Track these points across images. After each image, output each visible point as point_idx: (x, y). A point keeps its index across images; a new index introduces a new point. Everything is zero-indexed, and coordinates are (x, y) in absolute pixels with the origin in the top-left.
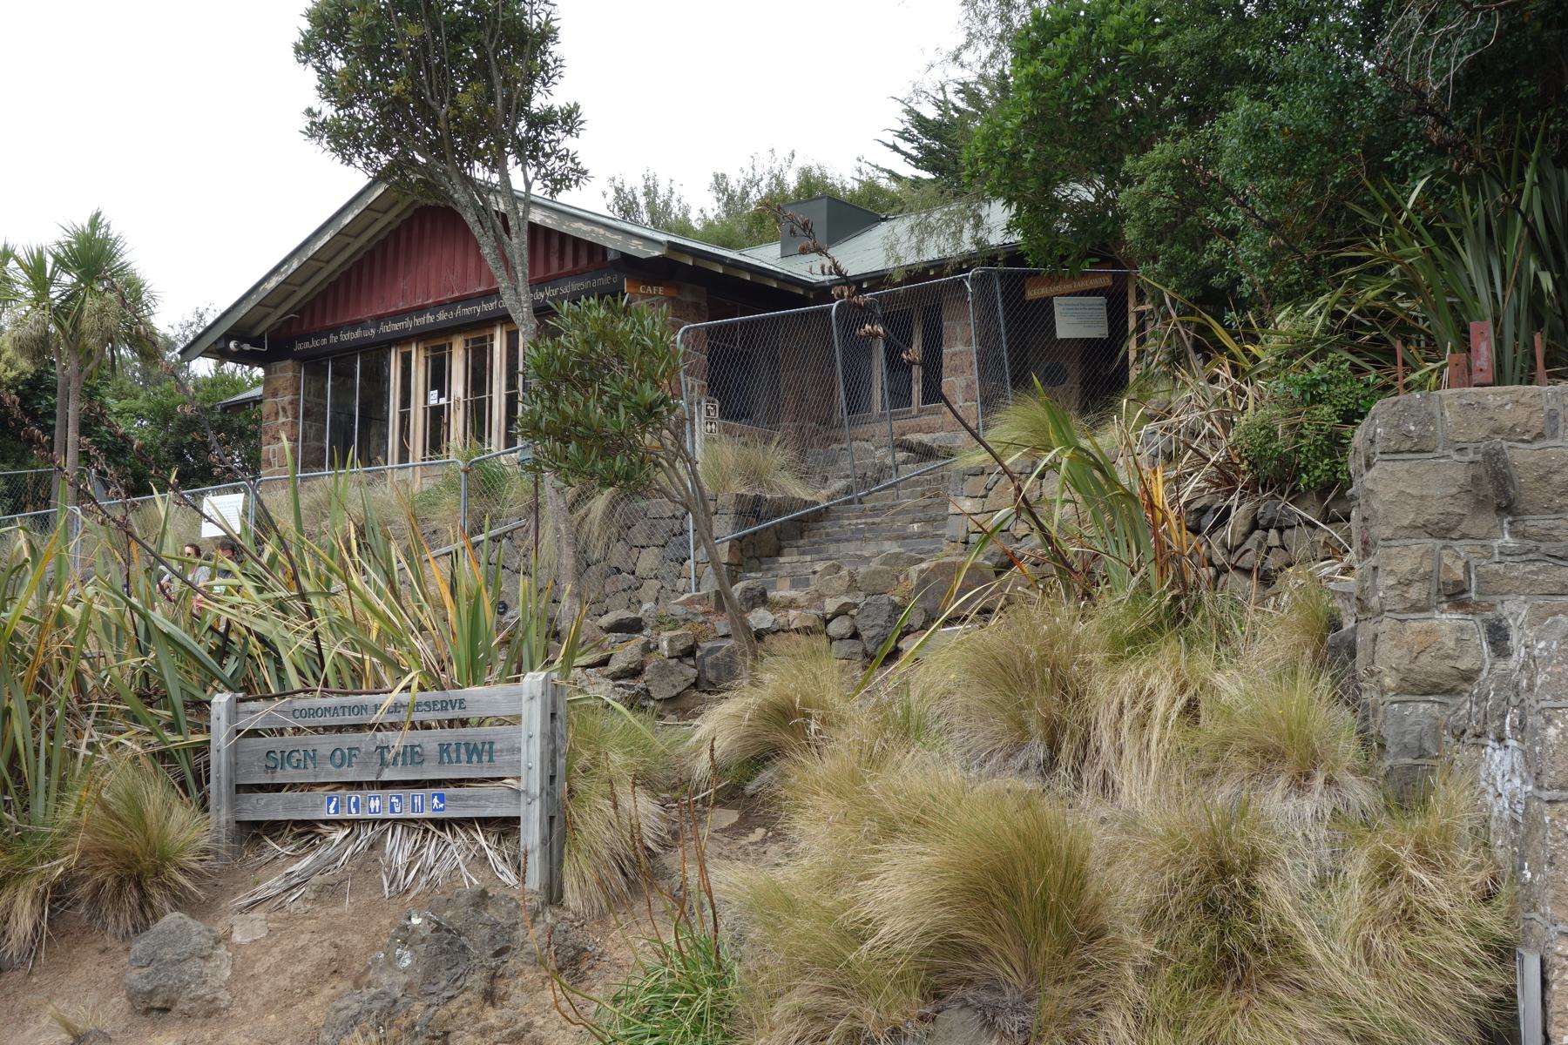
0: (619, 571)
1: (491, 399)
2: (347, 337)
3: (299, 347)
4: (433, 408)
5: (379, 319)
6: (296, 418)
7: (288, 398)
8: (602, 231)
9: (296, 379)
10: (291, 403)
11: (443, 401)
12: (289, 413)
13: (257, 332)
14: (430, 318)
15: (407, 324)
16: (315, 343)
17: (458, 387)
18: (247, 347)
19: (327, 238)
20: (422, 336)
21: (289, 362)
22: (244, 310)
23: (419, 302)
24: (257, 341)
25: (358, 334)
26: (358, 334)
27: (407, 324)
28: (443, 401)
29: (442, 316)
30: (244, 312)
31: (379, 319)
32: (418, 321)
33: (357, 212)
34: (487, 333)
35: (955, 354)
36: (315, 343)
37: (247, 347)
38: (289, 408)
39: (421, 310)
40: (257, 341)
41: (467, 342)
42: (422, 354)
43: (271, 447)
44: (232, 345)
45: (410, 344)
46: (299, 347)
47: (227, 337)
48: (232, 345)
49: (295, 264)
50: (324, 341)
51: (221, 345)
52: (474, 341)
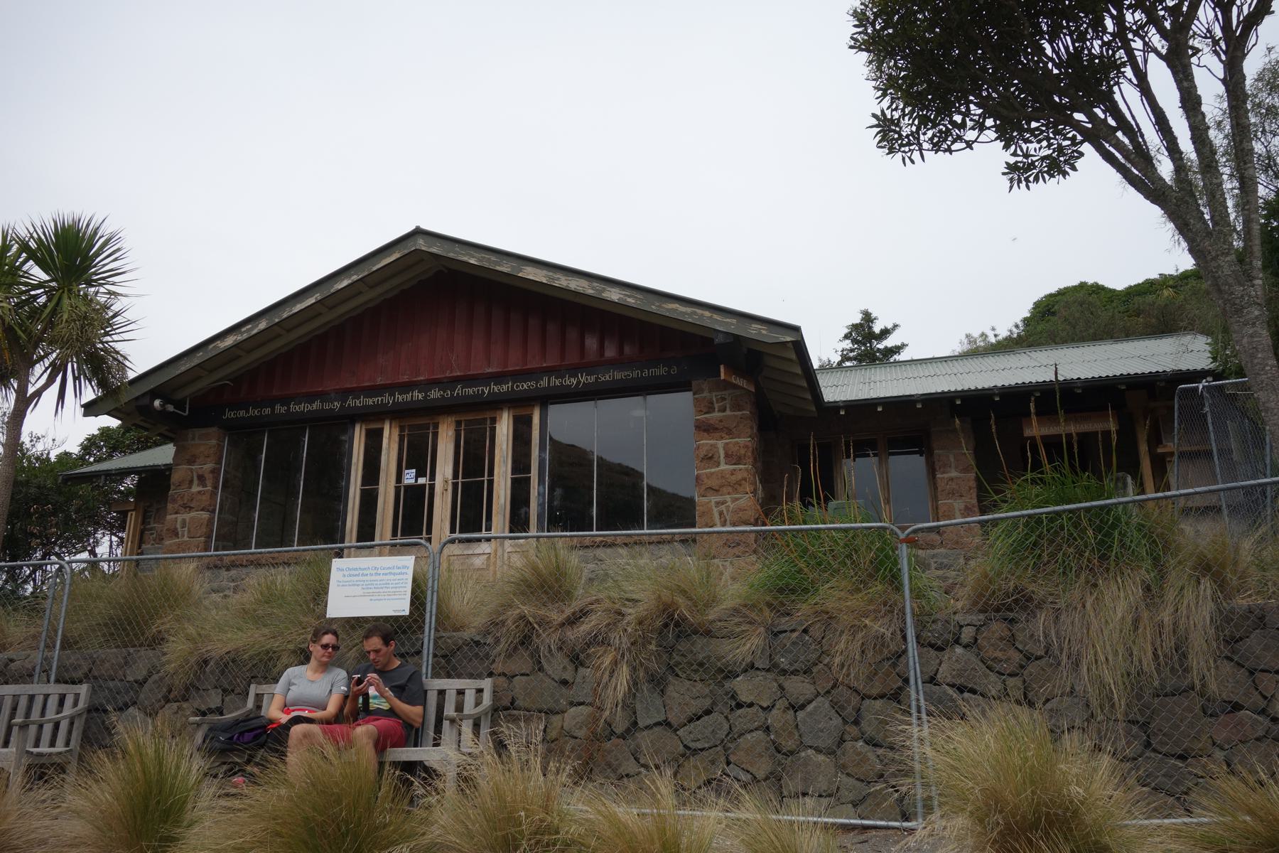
0: (1237, 707)
1: (491, 483)
2: (296, 408)
3: (230, 415)
4: (409, 488)
5: (345, 393)
6: (216, 487)
7: (209, 466)
8: (707, 314)
9: (220, 448)
10: (213, 471)
11: (421, 481)
12: (209, 483)
13: (179, 395)
14: (417, 395)
15: (387, 399)
16: (254, 412)
17: (445, 468)
18: (170, 408)
19: (311, 301)
20: (397, 414)
21: (215, 429)
22: (183, 367)
23: (405, 378)
24: (179, 405)
25: (316, 405)
26: (316, 405)
27: (387, 399)
28: (421, 481)
29: (435, 394)
30: (183, 369)
31: (345, 393)
32: (400, 398)
33: (355, 278)
34: (488, 415)
35: (952, 479)
36: (254, 412)
37: (170, 408)
38: (209, 477)
39: (407, 387)
40: (179, 405)
41: (458, 423)
42: (396, 433)
43: (180, 517)
44: (157, 403)
45: (383, 421)
46: (230, 415)
47: (154, 394)
48: (157, 403)
49: (263, 325)
50: (267, 411)
51: (146, 401)
52: (468, 423)
